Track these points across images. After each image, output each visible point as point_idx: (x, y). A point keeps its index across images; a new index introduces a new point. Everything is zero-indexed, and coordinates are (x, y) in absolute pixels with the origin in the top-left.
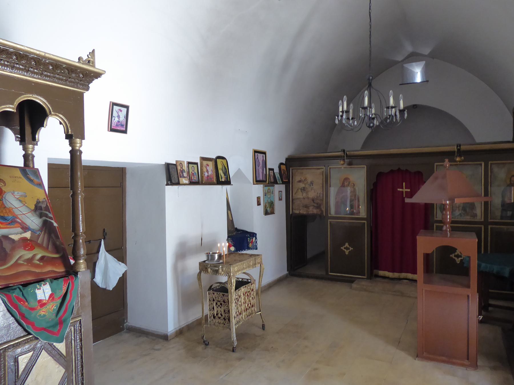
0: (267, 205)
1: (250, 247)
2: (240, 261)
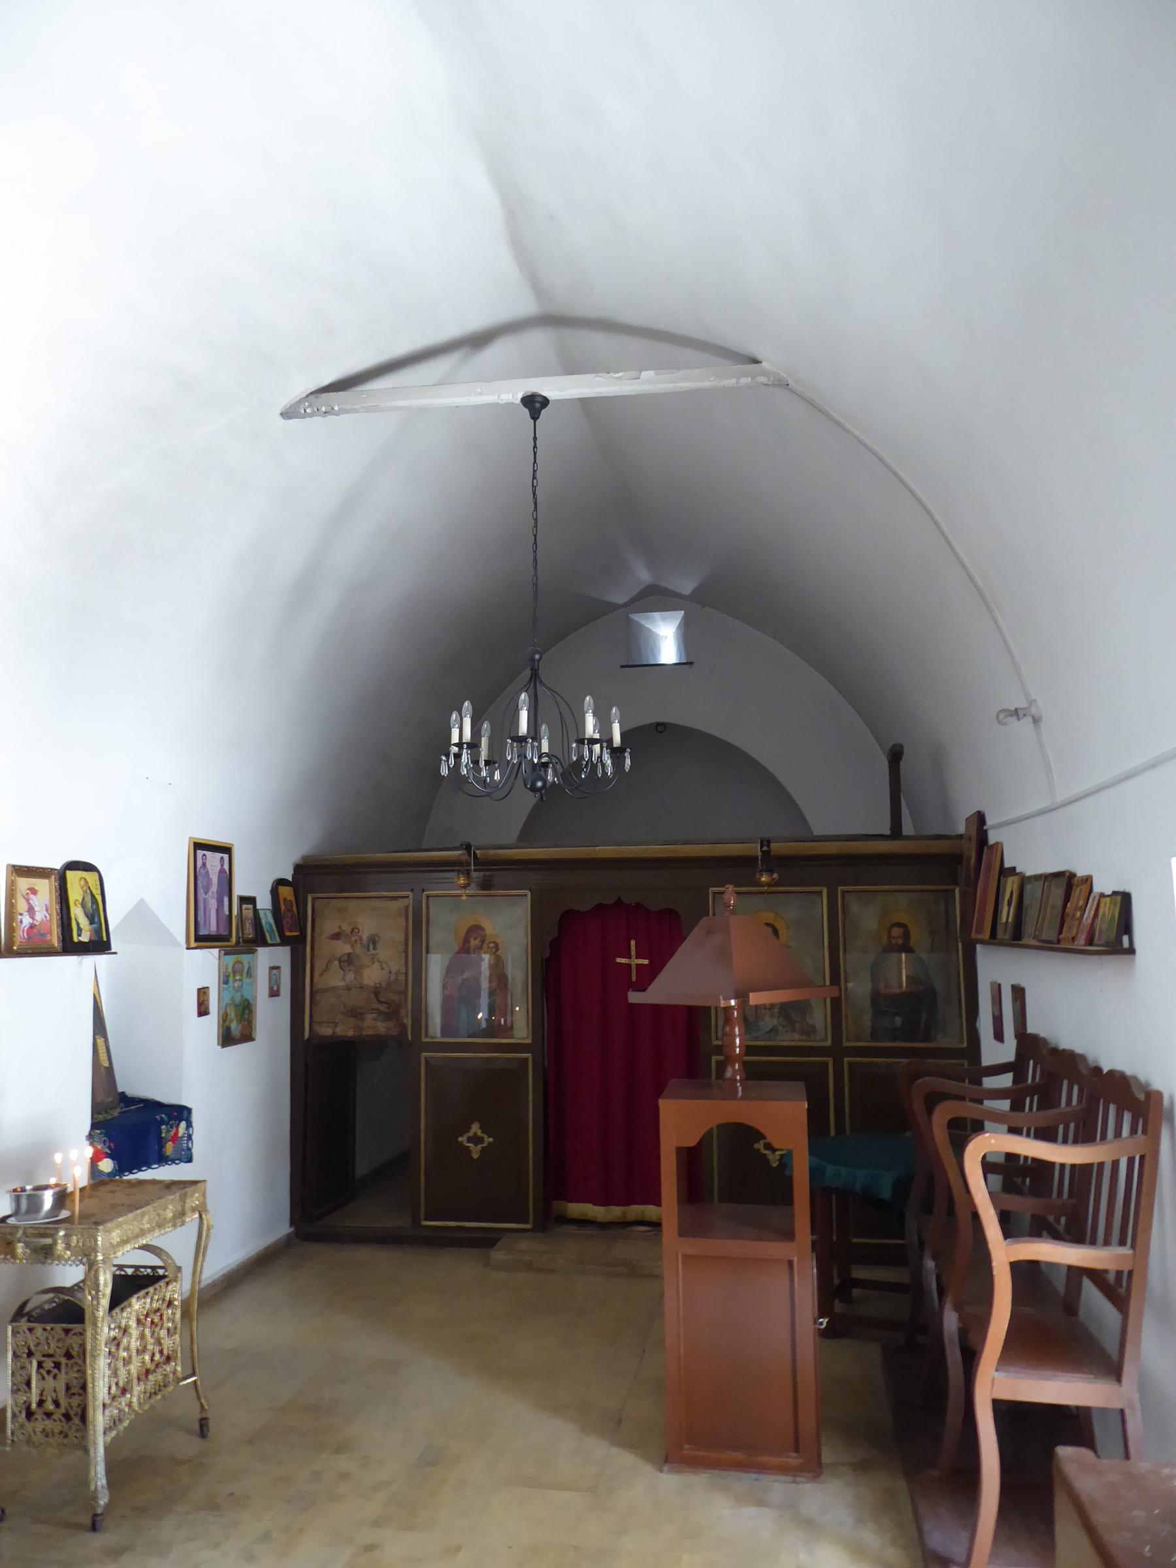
0: (232, 1014)
1: (168, 1157)
2: (132, 1208)
